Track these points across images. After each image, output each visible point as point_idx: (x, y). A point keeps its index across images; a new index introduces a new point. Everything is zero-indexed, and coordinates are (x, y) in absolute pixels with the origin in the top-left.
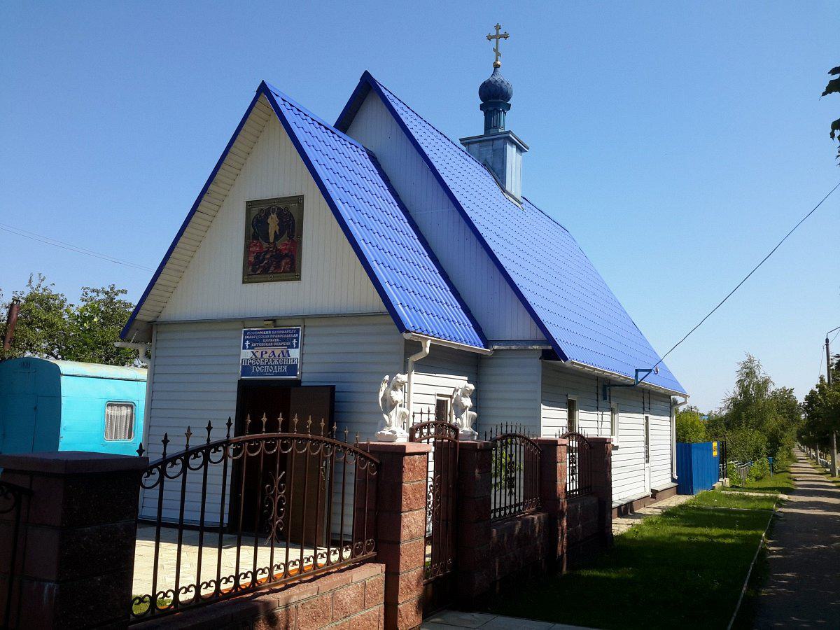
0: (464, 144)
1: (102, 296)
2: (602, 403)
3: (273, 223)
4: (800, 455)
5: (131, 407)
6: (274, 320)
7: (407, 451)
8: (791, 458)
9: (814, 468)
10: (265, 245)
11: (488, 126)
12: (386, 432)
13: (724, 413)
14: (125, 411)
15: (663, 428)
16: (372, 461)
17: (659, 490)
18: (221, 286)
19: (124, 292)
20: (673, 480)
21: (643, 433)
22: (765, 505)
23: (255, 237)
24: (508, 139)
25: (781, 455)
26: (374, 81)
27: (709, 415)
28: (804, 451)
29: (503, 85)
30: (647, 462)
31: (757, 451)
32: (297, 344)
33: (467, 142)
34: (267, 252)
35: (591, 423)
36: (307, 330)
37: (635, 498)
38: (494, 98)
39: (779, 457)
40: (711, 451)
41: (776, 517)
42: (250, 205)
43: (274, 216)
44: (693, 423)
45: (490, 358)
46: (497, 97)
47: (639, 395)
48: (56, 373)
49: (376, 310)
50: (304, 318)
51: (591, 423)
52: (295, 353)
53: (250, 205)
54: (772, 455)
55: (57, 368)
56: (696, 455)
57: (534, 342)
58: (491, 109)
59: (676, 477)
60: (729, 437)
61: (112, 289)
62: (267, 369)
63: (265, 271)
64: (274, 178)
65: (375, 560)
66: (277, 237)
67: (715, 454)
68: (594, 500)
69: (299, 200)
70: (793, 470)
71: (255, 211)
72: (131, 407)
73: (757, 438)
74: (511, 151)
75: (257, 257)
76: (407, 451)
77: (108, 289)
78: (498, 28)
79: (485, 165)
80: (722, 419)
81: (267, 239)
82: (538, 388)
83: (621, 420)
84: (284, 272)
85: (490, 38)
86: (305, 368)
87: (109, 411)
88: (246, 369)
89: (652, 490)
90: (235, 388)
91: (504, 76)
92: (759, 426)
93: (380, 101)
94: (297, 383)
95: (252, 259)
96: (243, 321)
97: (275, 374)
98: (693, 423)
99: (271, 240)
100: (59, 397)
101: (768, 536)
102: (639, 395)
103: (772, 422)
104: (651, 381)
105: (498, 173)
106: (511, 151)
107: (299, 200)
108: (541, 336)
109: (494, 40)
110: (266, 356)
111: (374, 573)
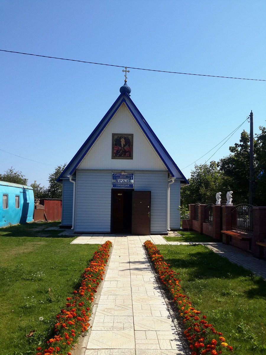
3: (123, 142)
10: (120, 148)
23: (116, 145)
34: (121, 150)
42: (114, 135)
43: (123, 139)
49: (165, 170)
52: (132, 181)
63: (120, 156)
66: (124, 146)
71: (116, 137)
72: (18, 197)
75: (117, 151)
81: (120, 145)
85: (123, 71)
88: (114, 185)
90: (111, 190)
91: (129, 85)
95: (115, 151)
96: (112, 170)
97: (125, 187)
99: (122, 146)
108: (180, 177)
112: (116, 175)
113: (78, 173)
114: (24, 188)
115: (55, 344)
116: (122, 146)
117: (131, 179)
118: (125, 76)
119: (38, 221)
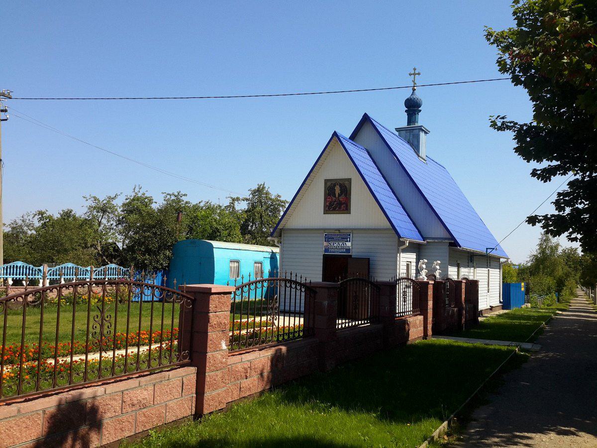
0: (397, 131)
1: (173, 198)
2: (470, 264)
3: (338, 190)
4: (582, 293)
5: (238, 262)
6: (339, 230)
7: (213, 291)
8: (572, 294)
9: (587, 301)
10: (334, 198)
11: (409, 122)
12: (421, 277)
13: (529, 264)
14: (260, 265)
15: (496, 275)
16: (188, 298)
17: (494, 306)
18: (313, 214)
19: (185, 195)
20: (500, 302)
21: (487, 278)
22: (548, 314)
23: (329, 195)
24: (420, 129)
25: (565, 292)
26: (369, 117)
27: (519, 265)
28: (583, 291)
29: (418, 101)
30: (488, 292)
31: (549, 289)
32: (350, 240)
33: (398, 130)
34: (335, 201)
35: (467, 273)
36: (354, 235)
37: (483, 309)
38: (413, 107)
39: (563, 293)
40: (521, 287)
41: (552, 319)
42: (326, 181)
43: (338, 186)
44: (509, 271)
45: (424, 245)
46: (415, 107)
47: (486, 259)
48: (211, 247)
49: (388, 227)
50: (353, 230)
51: (467, 273)
52: (349, 244)
53: (326, 181)
54: (559, 291)
55: (211, 245)
56: (513, 291)
57: (446, 239)
58: (411, 113)
59: (502, 301)
60: (532, 280)
61: (178, 194)
62: (336, 250)
63: (334, 209)
64: (338, 170)
65: (420, 315)
66: (339, 195)
67: (523, 289)
68: (472, 305)
69: (349, 180)
70: (572, 301)
71: (329, 184)
72: (261, 263)
73: (549, 281)
74: (422, 134)
75: (330, 203)
76: (213, 291)
77: (176, 194)
78: (415, 69)
79: (408, 142)
80: (528, 268)
81: (335, 196)
82: (447, 258)
83: (478, 271)
84: (343, 210)
85: (410, 75)
86: (353, 250)
87: (256, 265)
88: (326, 250)
89: (490, 306)
90: (322, 257)
91: (420, 95)
92: (551, 274)
93: (371, 125)
94: (350, 256)
95: (328, 204)
96: (324, 230)
97: (340, 252)
98: (509, 271)
99: (337, 195)
100: (213, 258)
101: (546, 324)
102: (486, 259)
103: (560, 272)
104: (494, 253)
105: (416, 147)
106: (422, 134)
107: (349, 180)
108: (448, 236)
109: (413, 76)
110: (335, 245)
111: (421, 318)
112: (332, 235)
113: (284, 233)
114: (272, 252)
115: (16, 356)
116: (337, 195)
117: (347, 241)
118: (414, 81)
119: (526, 322)
